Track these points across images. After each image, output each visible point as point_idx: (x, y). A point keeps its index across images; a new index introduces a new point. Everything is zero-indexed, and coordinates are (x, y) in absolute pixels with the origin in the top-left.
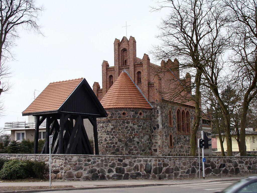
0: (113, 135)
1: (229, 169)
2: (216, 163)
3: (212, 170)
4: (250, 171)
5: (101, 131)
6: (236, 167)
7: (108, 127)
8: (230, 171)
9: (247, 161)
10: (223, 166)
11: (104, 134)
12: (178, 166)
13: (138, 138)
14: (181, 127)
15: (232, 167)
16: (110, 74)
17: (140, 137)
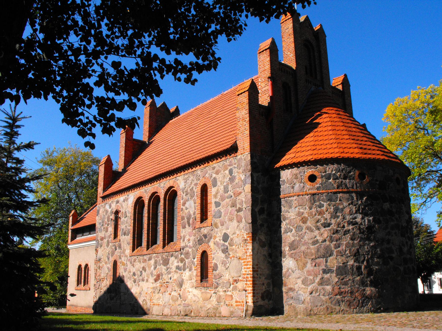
11: (395, 233)
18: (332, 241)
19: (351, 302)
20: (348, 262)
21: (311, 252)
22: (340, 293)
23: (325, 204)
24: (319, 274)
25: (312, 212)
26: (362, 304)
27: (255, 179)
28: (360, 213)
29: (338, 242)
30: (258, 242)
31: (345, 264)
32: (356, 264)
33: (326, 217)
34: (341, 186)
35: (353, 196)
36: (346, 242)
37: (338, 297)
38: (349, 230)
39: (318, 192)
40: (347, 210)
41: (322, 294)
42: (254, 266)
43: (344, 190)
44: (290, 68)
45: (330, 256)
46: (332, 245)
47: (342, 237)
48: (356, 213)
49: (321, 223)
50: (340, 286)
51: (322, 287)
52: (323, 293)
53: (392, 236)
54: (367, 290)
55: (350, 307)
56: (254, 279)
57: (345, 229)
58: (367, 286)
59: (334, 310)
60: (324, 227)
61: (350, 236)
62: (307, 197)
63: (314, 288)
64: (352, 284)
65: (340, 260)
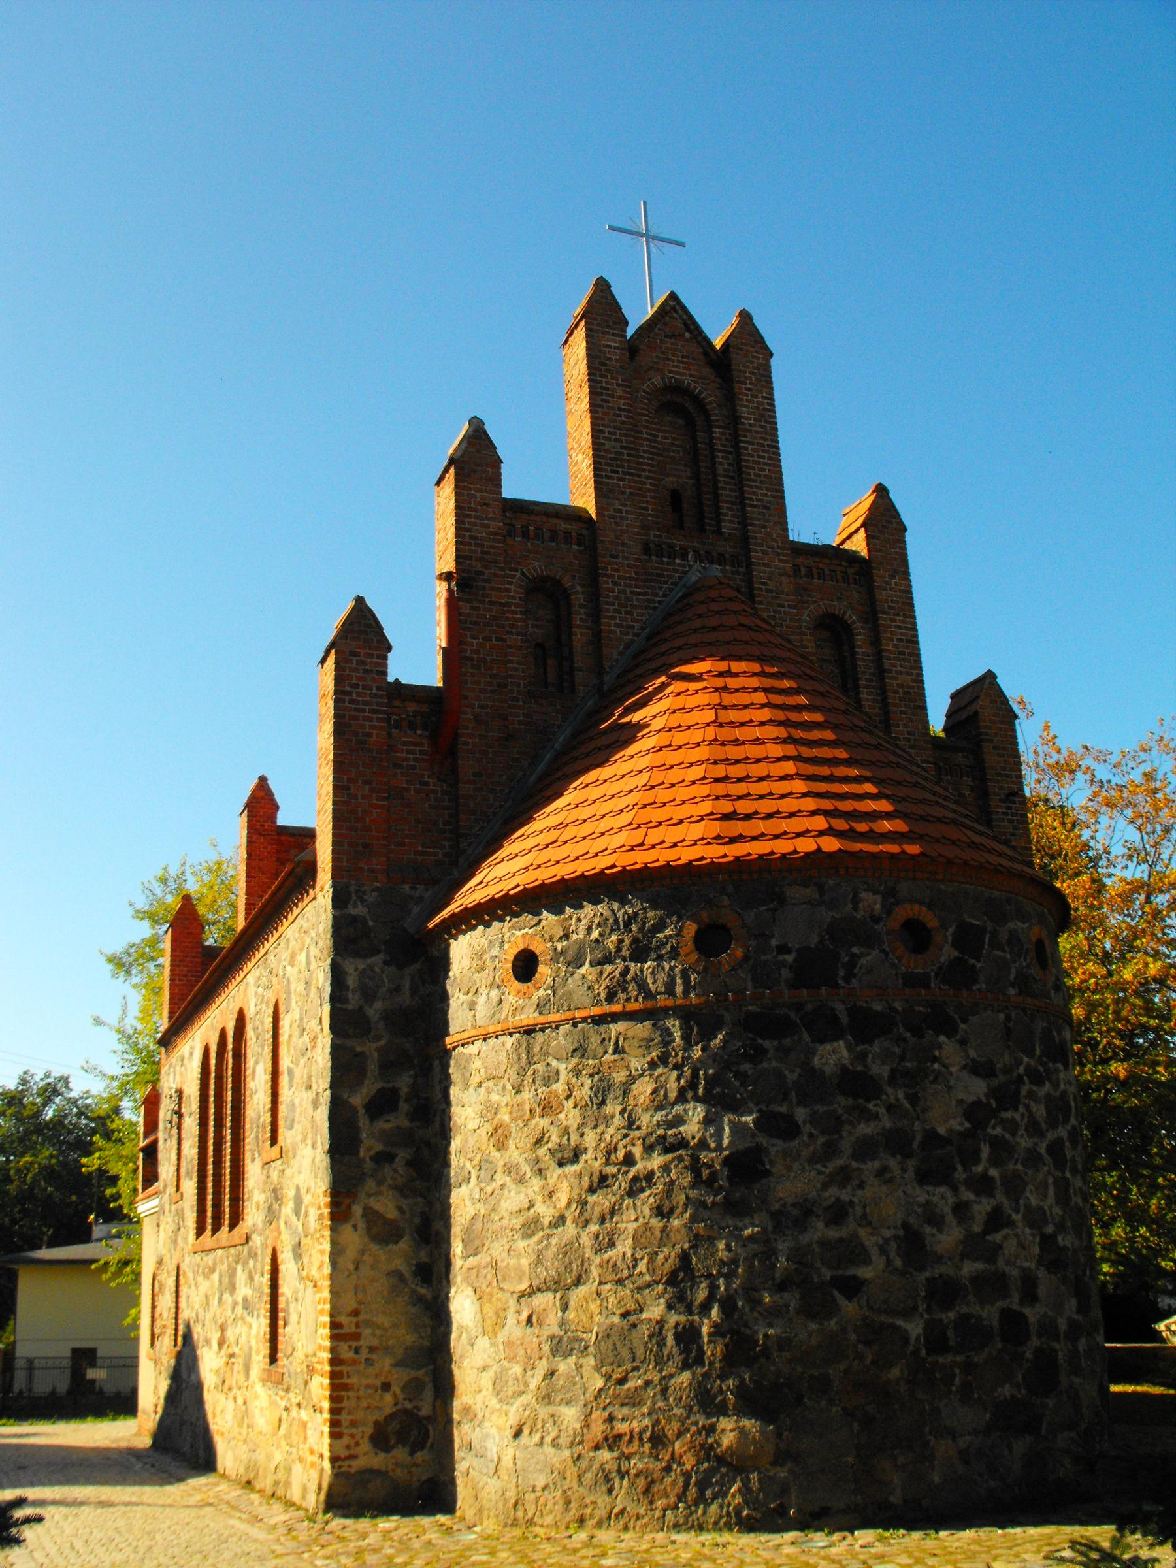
0: (983, 1186)
11: (881, 1173)
18: (587, 1222)
19: (653, 1482)
20: (641, 1311)
21: (518, 1268)
22: (612, 1441)
23: (562, 1067)
24: (541, 1358)
25: (523, 1103)
26: (701, 1492)
27: (351, 982)
28: (697, 1099)
29: (607, 1225)
30: (361, 1224)
31: (632, 1318)
32: (673, 1318)
33: (565, 1123)
34: (625, 990)
35: (668, 1029)
36: (635, 1225)
37: (605, 1455)
38: (650, 1176)
39: (542, 1019)
40: (643, 1089)
41: (548, 1439)
42: (338, 1319)
43: (633, 1006)
44: (575, 515)
45: (578, 1282)
46: (586, 1240)
47: (621, 1204)
48: (681, 1098)
49: (550, 1145)
50: (610, 1409)
51: (551, 1409)
52: (553, 1435)
53: (861, 1186)
54: (723, 1430)
55: (651, 1502)
56: (338, 1369)
57: (633, 1171)
58: (722, 1411)
59: (588, 1511)
60: (561, 1164)
61: (652, 1200)
62: (509, 1041)
63: (527, 1413)
64: (660, 1404)
65: (611, 1300)
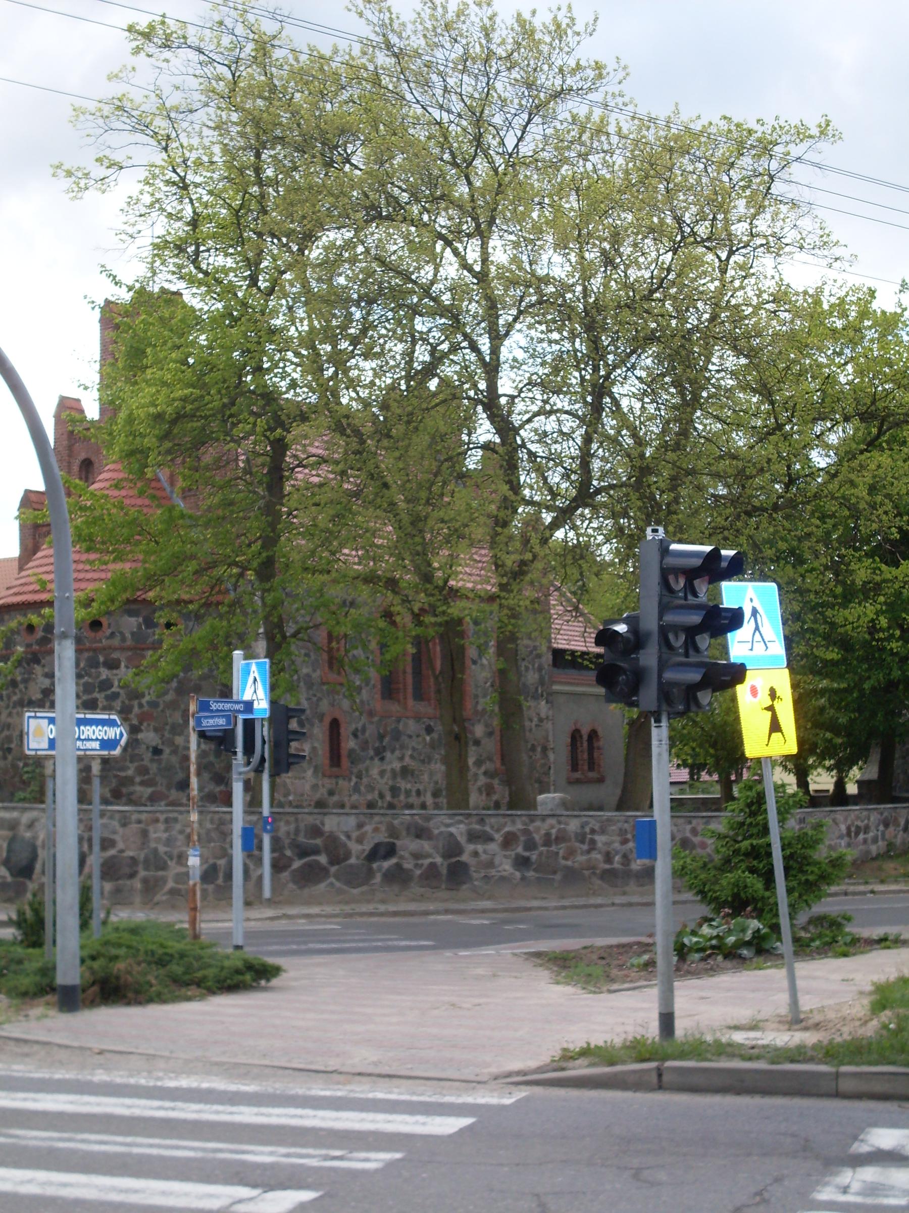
1: (416, 866)
2: (349, 837)
3: (333, 869)
4: (523, 878)
5: (9, 697)
6: (454, 860)
7: (32, 685)
8: (420, 876)
9: (508, 833)
10: (387, 850)
12: (162, 849)
13: (156, 730)
14: (405, 685)
15: (428, 856)
16: (83, 456)
17: (168, 727)
